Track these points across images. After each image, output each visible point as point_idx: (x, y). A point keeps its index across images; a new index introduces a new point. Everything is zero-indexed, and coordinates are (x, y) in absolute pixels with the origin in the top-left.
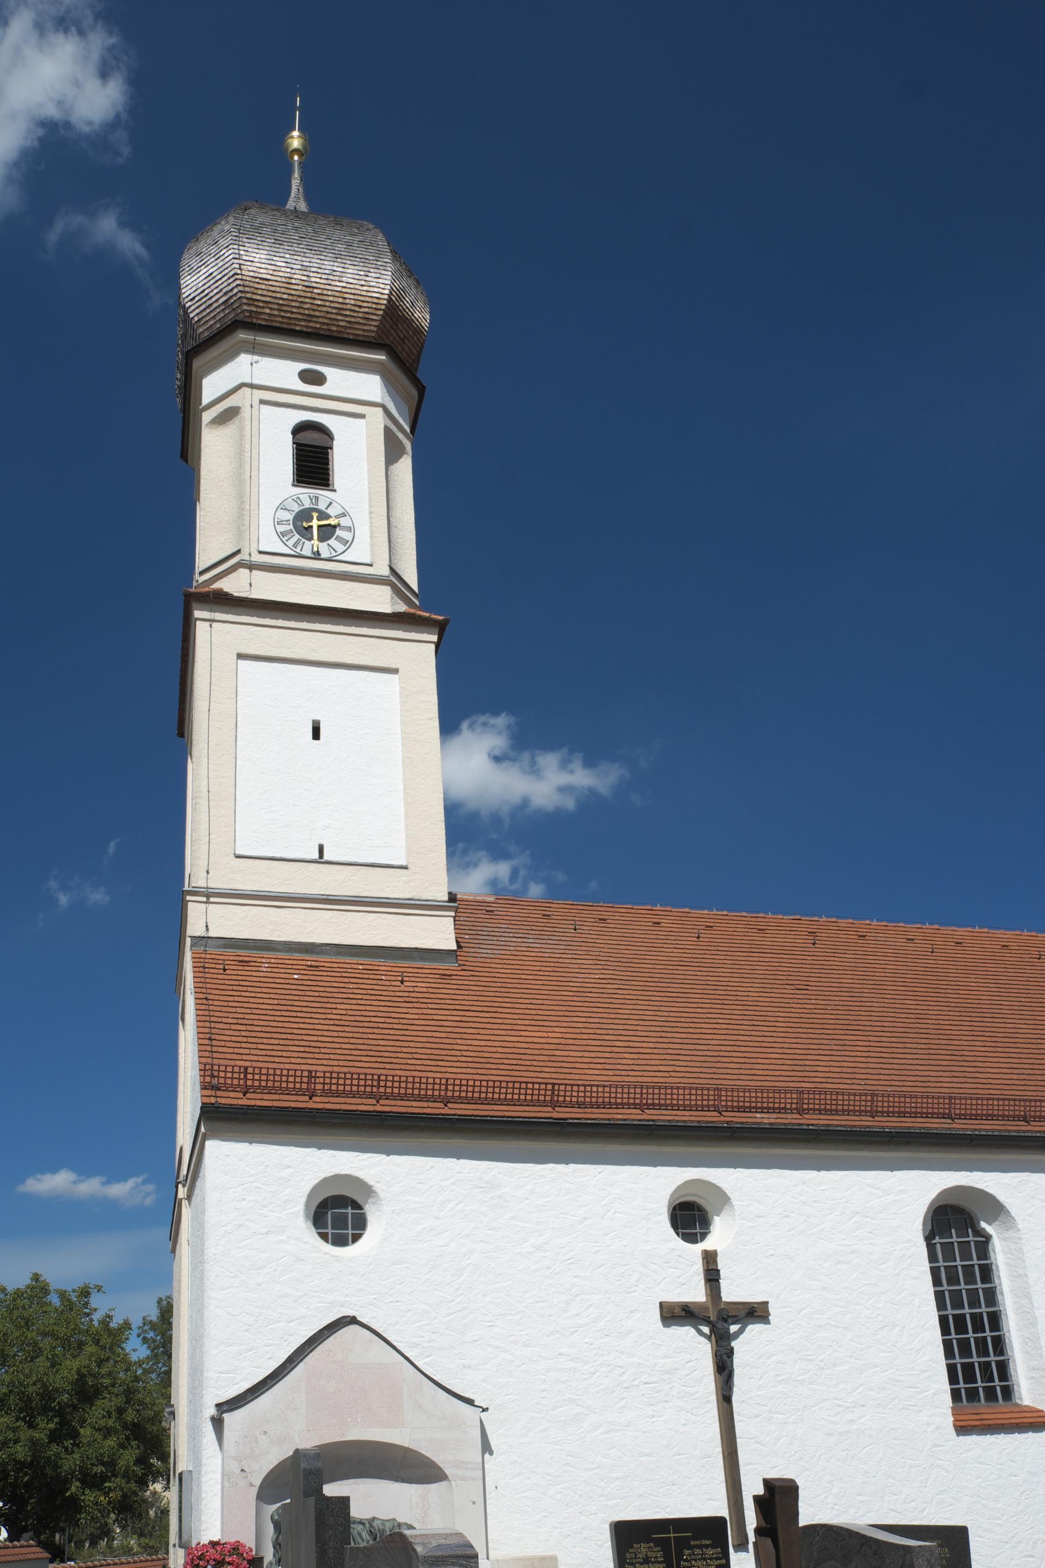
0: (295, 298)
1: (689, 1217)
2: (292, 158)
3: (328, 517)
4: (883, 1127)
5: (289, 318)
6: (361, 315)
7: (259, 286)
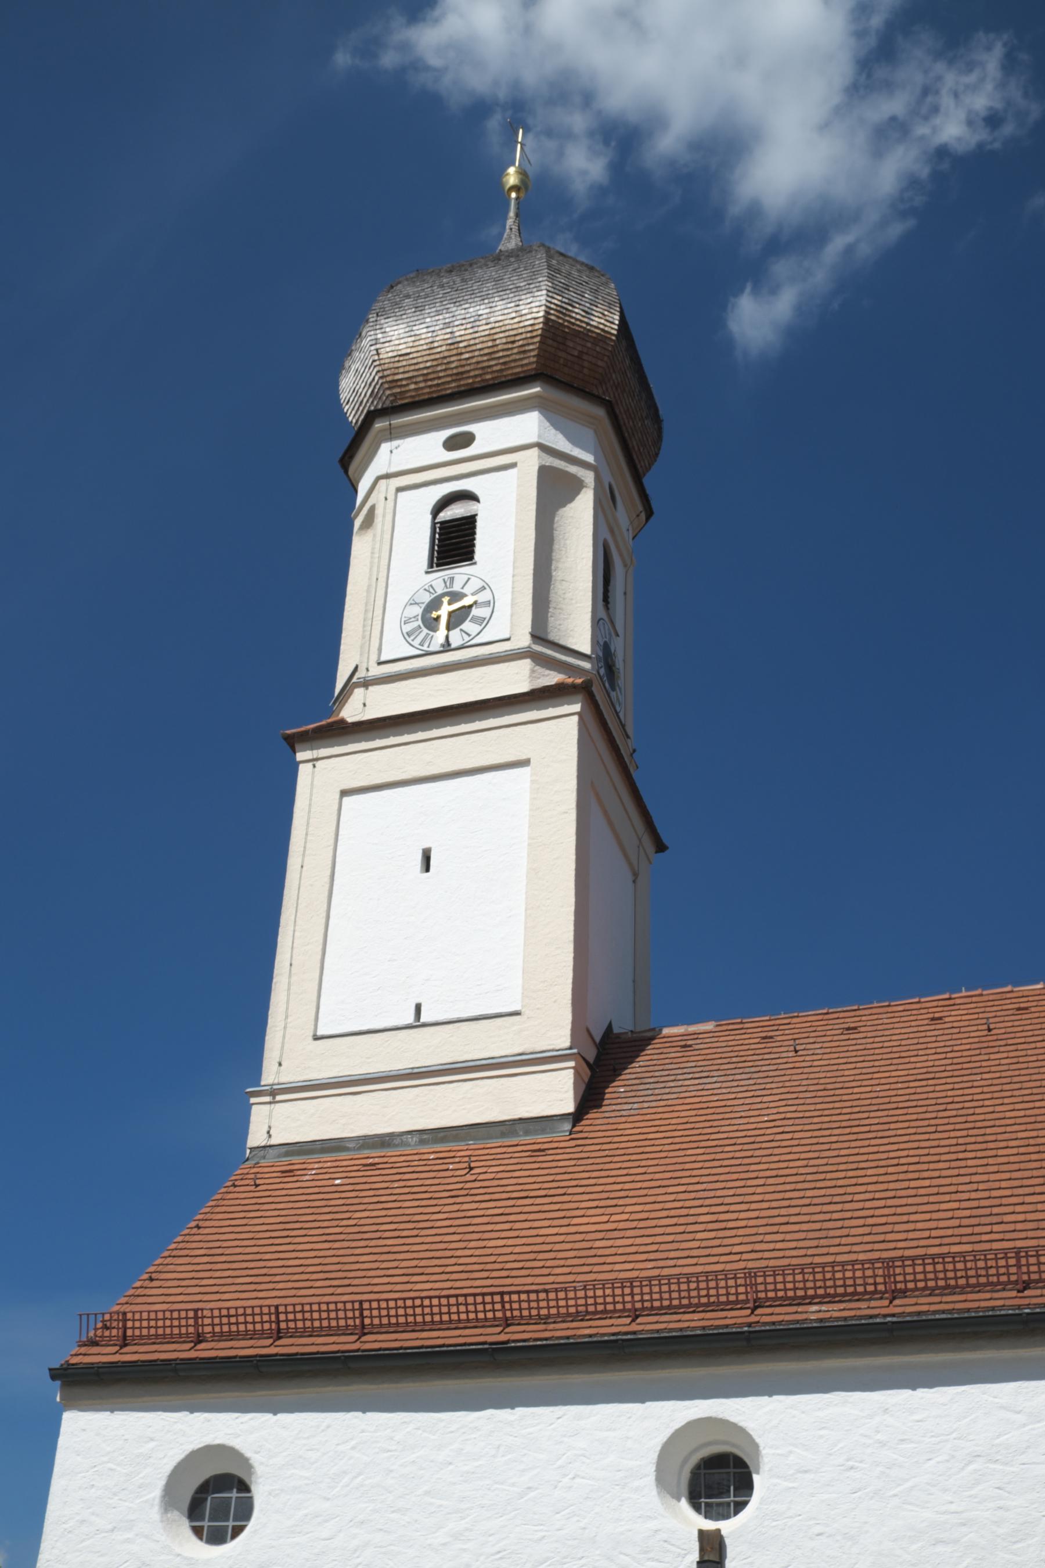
0: (440, 362)
2: (509, 196)
3: (464, 595)
4: (1019, 1307)
5: (438, 385)
6: (515, 351)
7: (400, 364)
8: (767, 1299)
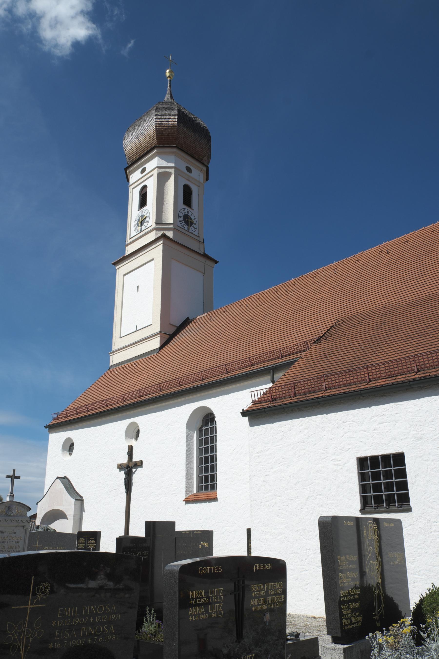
8: (255, 364)
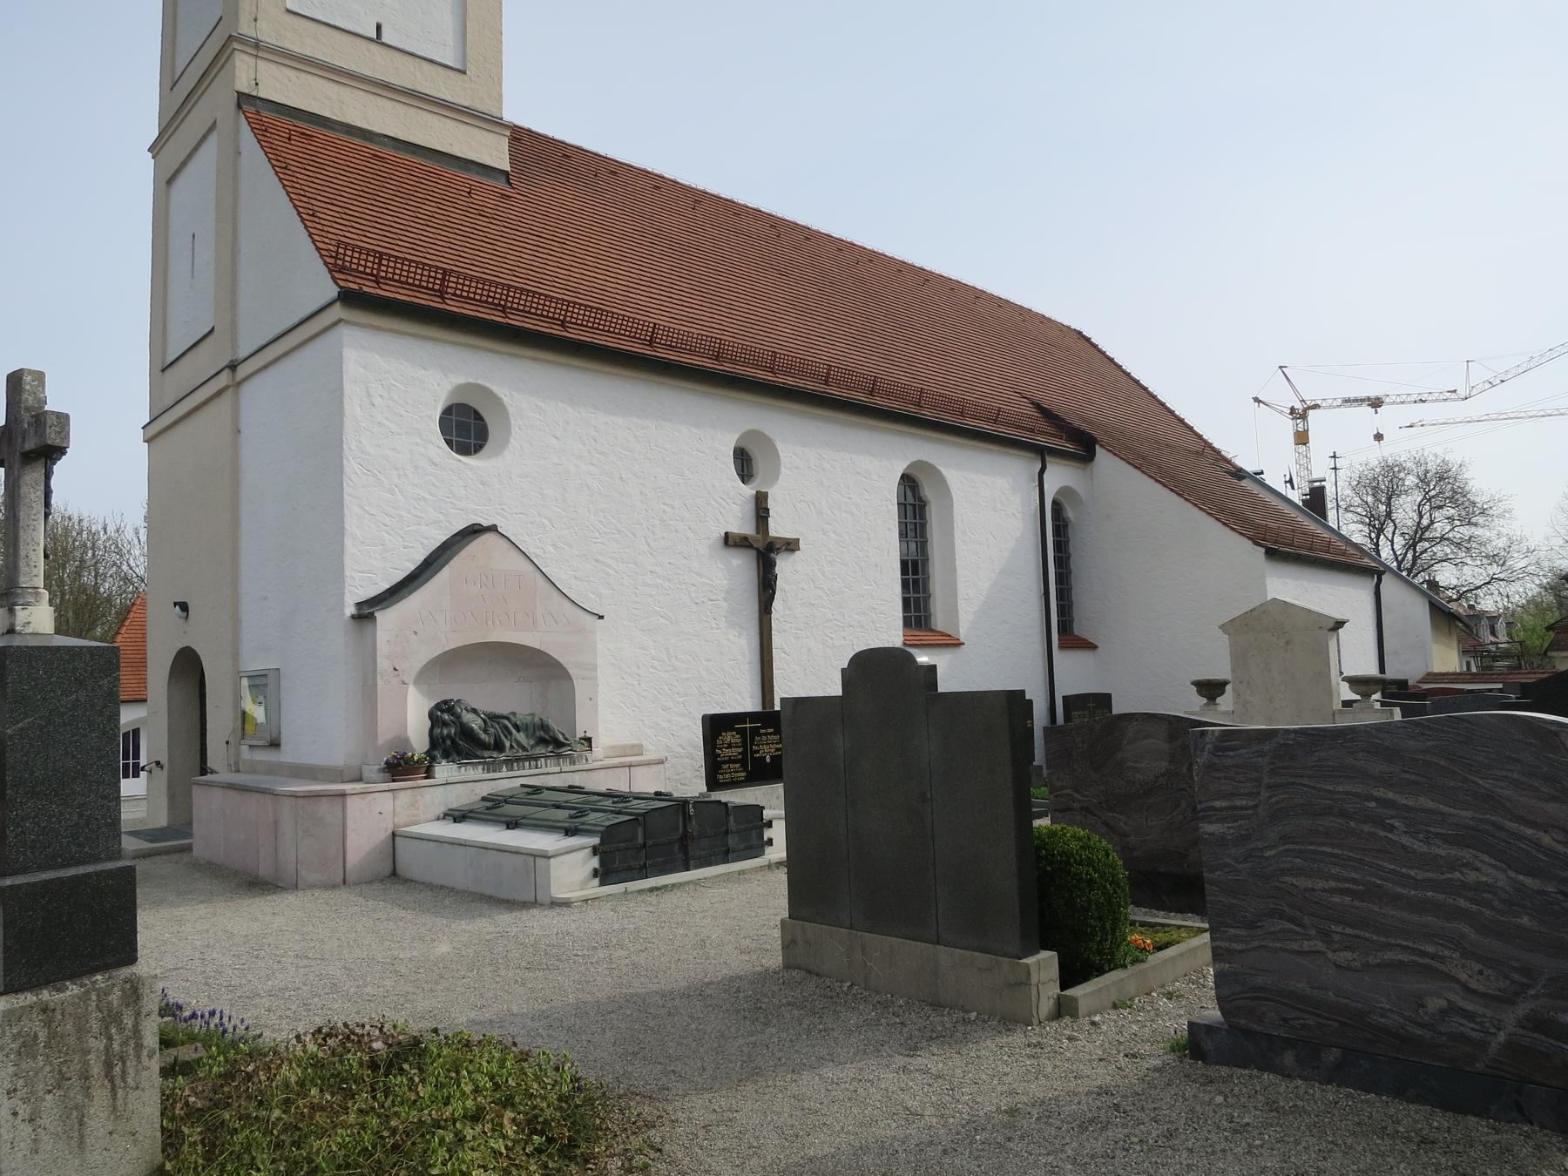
1: (744, 463)
